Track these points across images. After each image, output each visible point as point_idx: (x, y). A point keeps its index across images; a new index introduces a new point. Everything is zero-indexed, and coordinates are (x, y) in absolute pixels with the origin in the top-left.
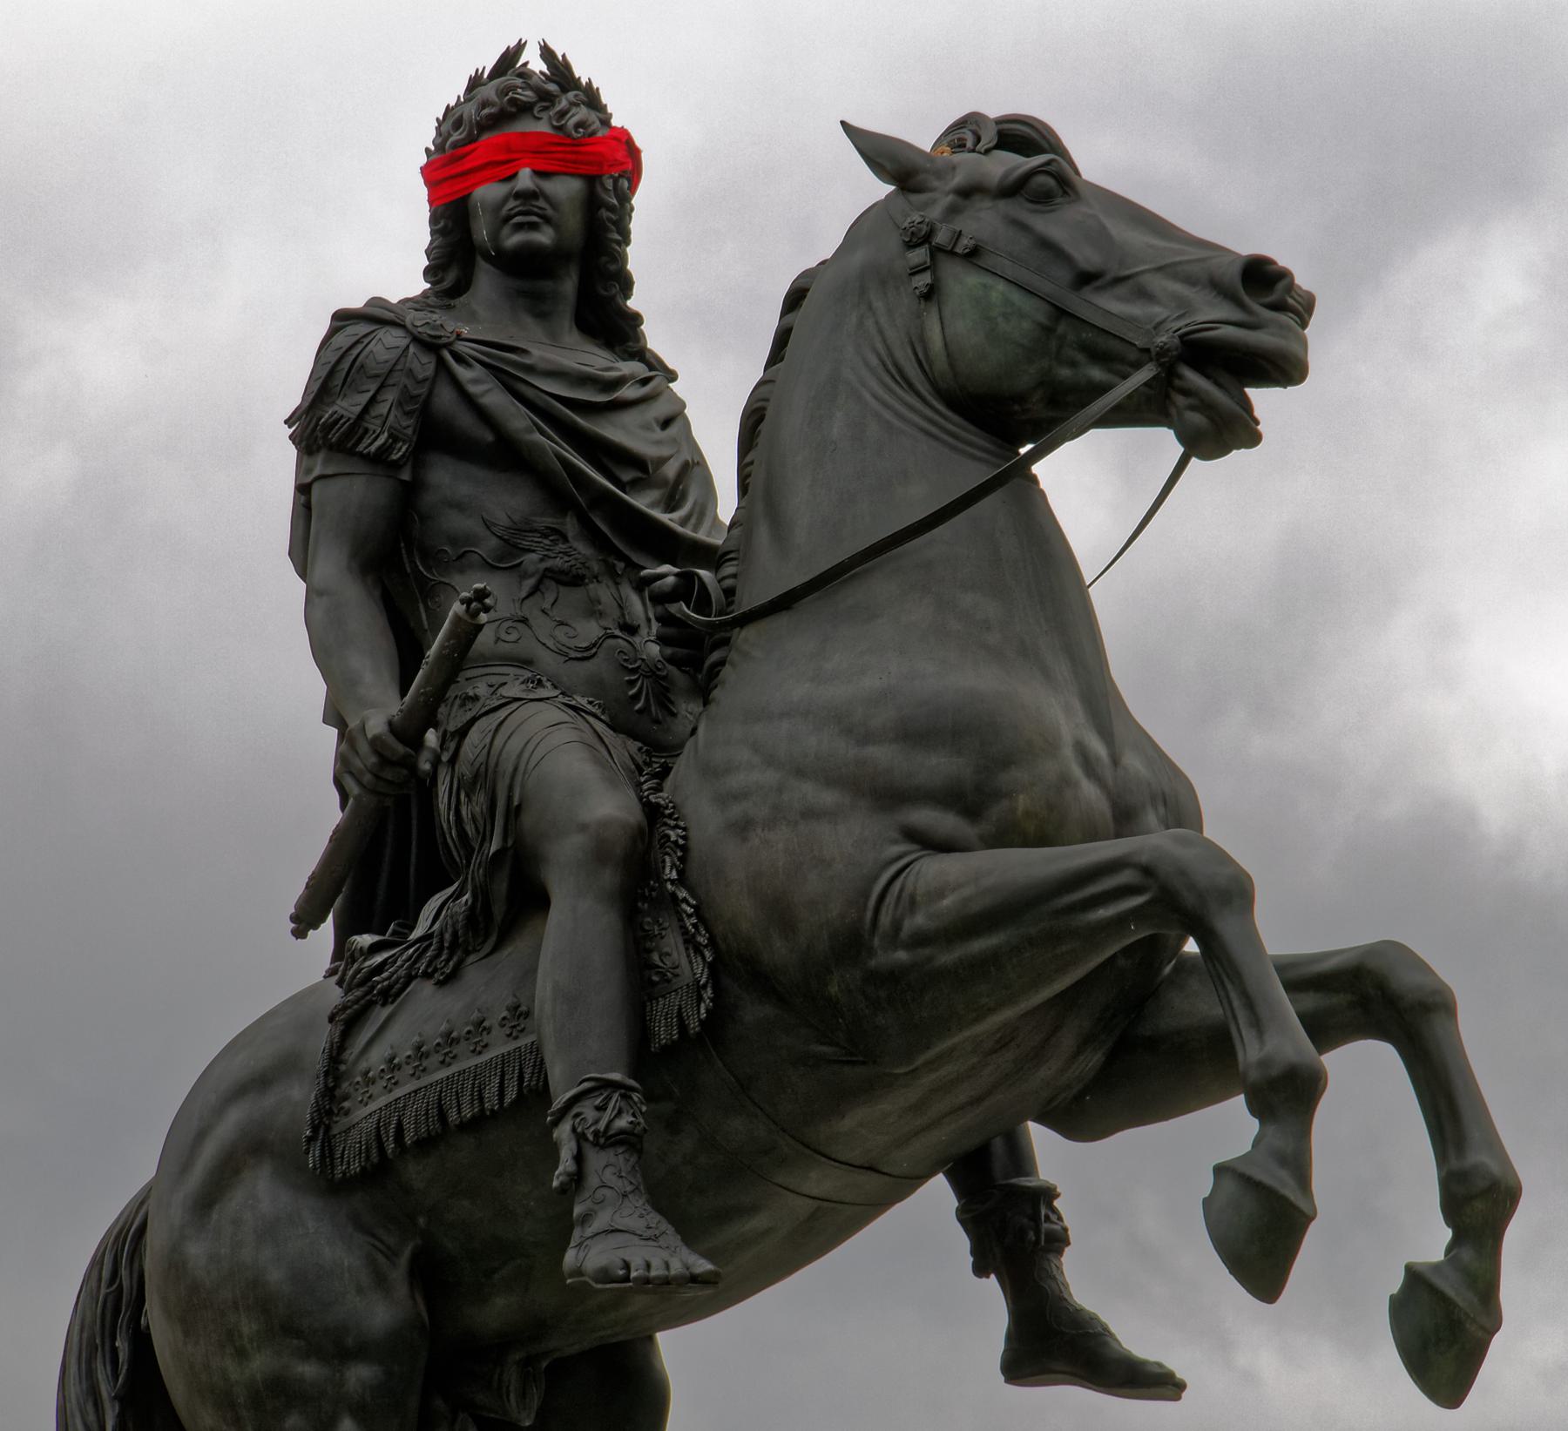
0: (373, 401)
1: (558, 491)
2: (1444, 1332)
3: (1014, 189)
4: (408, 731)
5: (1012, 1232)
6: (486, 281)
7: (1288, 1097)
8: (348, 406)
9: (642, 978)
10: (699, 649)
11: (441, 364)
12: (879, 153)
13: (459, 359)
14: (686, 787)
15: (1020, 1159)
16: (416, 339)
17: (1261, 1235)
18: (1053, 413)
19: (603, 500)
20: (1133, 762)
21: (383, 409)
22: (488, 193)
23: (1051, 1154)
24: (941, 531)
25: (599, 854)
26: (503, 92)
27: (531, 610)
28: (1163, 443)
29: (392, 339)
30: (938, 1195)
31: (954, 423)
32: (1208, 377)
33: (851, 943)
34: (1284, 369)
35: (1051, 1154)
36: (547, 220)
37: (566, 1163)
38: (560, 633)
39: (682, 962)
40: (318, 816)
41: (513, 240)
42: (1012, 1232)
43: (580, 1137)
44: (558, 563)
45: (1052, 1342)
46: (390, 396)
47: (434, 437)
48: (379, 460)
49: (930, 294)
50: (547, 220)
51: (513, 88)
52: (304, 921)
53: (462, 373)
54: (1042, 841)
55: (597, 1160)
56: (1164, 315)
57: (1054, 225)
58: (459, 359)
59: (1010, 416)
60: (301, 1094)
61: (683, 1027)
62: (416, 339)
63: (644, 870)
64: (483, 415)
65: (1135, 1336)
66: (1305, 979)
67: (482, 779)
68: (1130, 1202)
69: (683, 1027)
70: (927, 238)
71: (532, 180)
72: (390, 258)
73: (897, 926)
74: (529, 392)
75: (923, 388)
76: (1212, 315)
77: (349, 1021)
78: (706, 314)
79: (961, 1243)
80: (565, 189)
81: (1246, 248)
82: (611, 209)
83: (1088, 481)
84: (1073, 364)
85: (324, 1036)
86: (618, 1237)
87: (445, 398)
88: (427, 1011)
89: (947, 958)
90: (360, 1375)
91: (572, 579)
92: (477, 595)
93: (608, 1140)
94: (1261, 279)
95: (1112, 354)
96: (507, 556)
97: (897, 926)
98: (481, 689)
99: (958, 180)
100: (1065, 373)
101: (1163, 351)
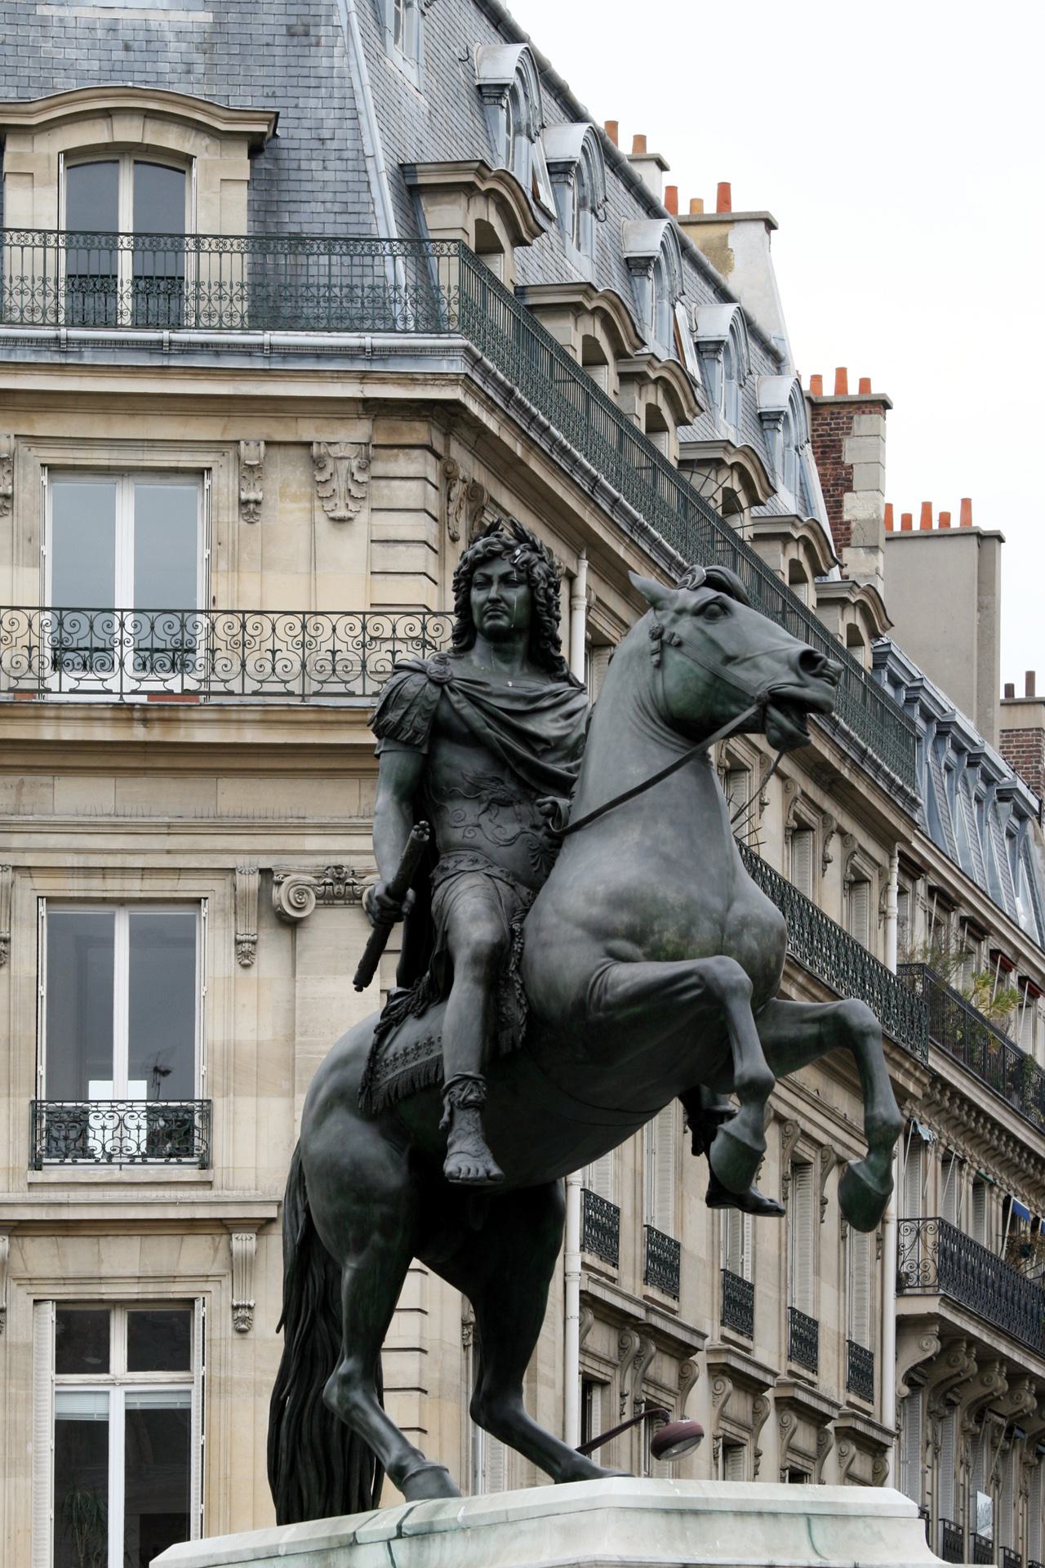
0: (406, 713)
1: (500, 758)
3: (702, 611)
6: (480, 645)
8: (393, 717)
11: (443, 692)
13: (452, 690)
16: (431, 680)
19: (523, 762)
21: (411, 717)
22: (477, 596)
24: (650, 790)
25: (476, 960)
26: (485, 545)
27: (484, 819)
29: (419, 679)
32: (782, 712)
33: (581, 1006)
36: (505, 613)
37: (446, 1118)
38: (497, 831)
41: (488, 624)
43: (452, 1104)
44: (500, 795)
46: (415, 711)
48: (408, 744)
49: (659, 665)
50: (505, 613)
51: (491, 544)
53: (453, 697)
55: (459, 1114)
58: (452, 690)
60: (361, 1066)
61: (514, 1044)
62: (431, 680)
63: (502, 964)
64: (461, 717)
69: (514, 1044)
70: (660, 635)
73: (599, 999)
74: (485, 706)
75: (653, 714)
80: (515, 595)
82: (542, 605)
84: (723, 704)
87: (445, 709)
89: (620, 1016)
90: (378, 1211)
91: (505, 803)
93: (466, 1105)
95: (739, 696)
96: (474, 792)
97: (599, 999)
98: (451, 864)
99: (677, 605)
100: (719, 708)
101: (759, 699)
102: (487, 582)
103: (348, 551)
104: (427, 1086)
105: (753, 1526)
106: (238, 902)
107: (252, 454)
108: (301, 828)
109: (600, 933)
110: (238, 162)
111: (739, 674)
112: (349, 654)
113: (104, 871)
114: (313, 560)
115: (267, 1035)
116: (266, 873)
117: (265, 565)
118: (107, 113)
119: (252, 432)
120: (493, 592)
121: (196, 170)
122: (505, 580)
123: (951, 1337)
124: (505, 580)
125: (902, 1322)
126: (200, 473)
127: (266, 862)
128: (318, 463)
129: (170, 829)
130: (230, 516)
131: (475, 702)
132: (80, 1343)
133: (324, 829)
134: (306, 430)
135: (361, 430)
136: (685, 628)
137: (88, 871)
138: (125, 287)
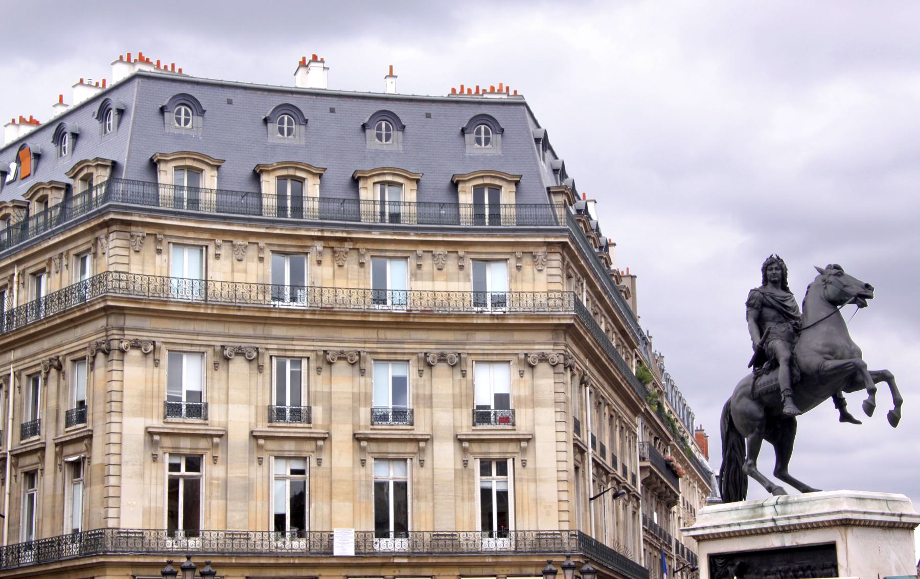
1: (780, 312)
2: (894, 418)
3: (836, 275)
4: (762, 344)
5: (840, 404)
6: (770, 284)
7: (872, 392)
8: (752, 302)
9: (792, 375)
10: (797, 331)
12: (819, 270)
14: (796, 350)
15: (841, 395)
17: (869, 408)
18: (842, 303)
20: (853, 347)
22: (769, 273)
23: (844, 394)
28: (855, 306)
30: (831, 399)
31: (829, 304)
33: (818, 372)
34: (871, 297)
35: (844, 394)
39: (796, 372)
40: (751, 353)
42: (840, 404)
45: (845, 417)
47: (764, 305)
48: (757, 308)
52: (750, 366)
54: (841, 359)
56: (855, 290)
57: (841, 279)
59: (835, 302)
60: (750, 388)
65: (856, 418)
66: (873, 374)
67: (771, 349)
68: (855, 400)
71: (775, 273)
72: (758, 282)
76: (862, 291)
77: (755, 379)
78: (799, 284)
79: (833, 405)
80: (779, 272)
81: (866, 282)
83: (847, 311)
85: (752, 381)
86: (789, 408)
88: (764, 379)
90: (758, 423)
91: (781, 322)
92: (770, 325)
93: (789, 396)
94: (867, 286)
95: (849, 295)
96: (773, 320)
102: (772, 269)
103: (542, 277)
104: (775, 391)
105: (875, 503)
106: (520, 361)
107: (519, 255)
108: (534, 343)
109: (821, 353)
110: (513, 188)
111: (848, 290)
112: (544, 301)
113: (488, 354)
114: (534, 280)
115: (527, 394)
116: (526, 354)
117: (522, 281)
118: (482, 177)
119: (519, 251)
120: (774, 271)
121: (503, 189)
122: (776, 269)
123: (652, 472)
124: (776, 269)
125: (641, 468)
126: (506, 260)
127: (526, 352)
128: (534, 257)
129: (503, 344)
130: (514, 270)
131: (773, 298)
132: (485, 470)
133: (539, 344)
134: (531, 249)
135: (544, 249)
136: (831, 279)
137: (484, 354)
138: (487, 217)
